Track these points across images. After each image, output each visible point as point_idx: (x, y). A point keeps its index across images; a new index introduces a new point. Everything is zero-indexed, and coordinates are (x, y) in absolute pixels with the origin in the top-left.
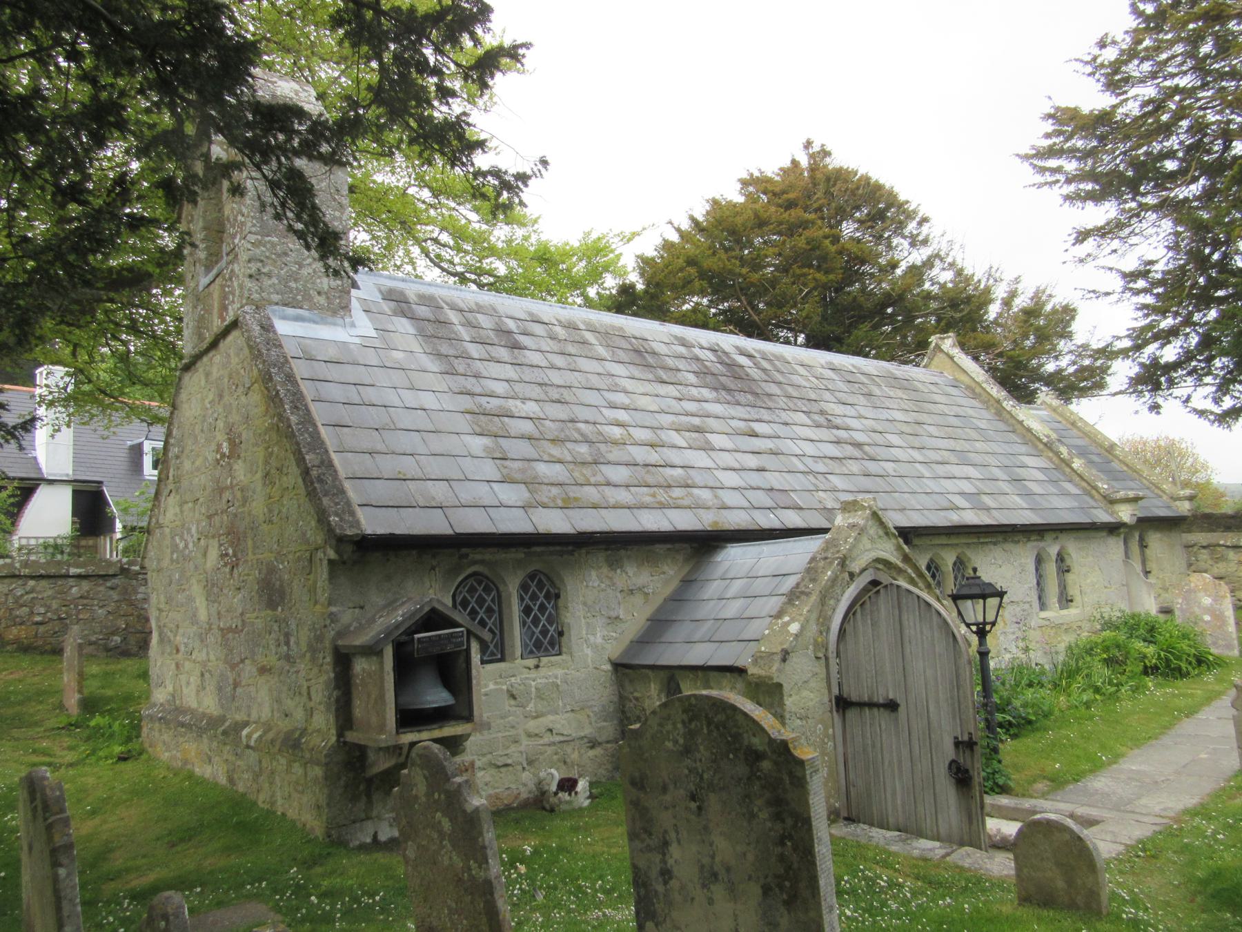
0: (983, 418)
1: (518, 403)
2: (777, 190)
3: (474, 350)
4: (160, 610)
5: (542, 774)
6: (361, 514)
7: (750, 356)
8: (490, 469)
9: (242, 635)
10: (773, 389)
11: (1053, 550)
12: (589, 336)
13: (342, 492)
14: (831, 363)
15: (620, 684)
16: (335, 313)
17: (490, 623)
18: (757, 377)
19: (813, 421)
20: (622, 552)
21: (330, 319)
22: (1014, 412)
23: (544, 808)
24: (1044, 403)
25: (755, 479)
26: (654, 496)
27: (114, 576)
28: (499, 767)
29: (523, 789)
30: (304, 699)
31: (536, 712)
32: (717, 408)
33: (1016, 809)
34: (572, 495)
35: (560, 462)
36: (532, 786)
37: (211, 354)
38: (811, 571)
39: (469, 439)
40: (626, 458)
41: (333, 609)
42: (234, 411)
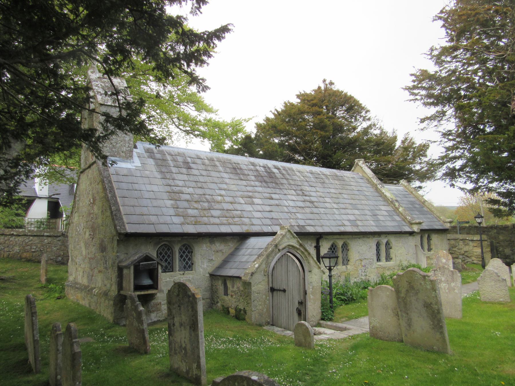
0: (369, 191)
1: (186, 188)
2: (309, 99)
3: (174, 170)
4: (72, 250)
7: (278, 169)
8: (172, 212)
11: (340, 243)
12: (217, 163)
13: (122, 219)
14: (311, 171)
15: (212, 281)
16: (127, 158)
18: (279, 177)
19: (297, 193)
20: (215, 239)
21: (126, 161)
24: (402, 184)
25: (267, 215)
26: (227, 221)
27: (60, 236)
30: (110, 281)
32: (260, 189)
33: (331, 326)
35: (197, 209)
39: (166, 201)
40: (220, 207)
41: (118, 254)
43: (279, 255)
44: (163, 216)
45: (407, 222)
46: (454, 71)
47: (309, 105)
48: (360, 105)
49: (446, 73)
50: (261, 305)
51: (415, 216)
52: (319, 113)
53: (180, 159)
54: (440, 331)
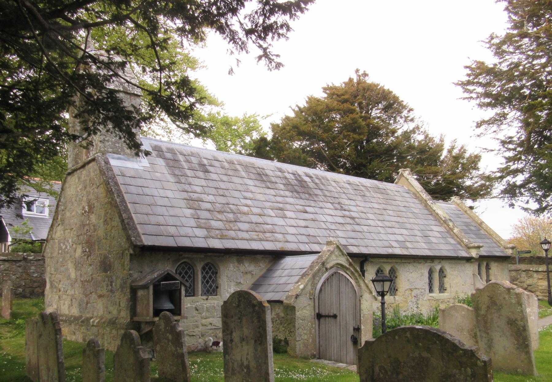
0: (417, 207)
1: (206, 196)
2: (339, 93)
3: (189, 173)
5: (207, 339)
6: (143, 237)
7: (320, 179)
8: (192, 223)
9: (91, 283)
10: (318, 192)
11: (438, 268)
12: (239, 167)
13: (136, 229)
17: (190, 281)
18: (311, 187)
19: (334, 207)
20: (244, 257)
21: (131, 159)
22: (432, 206)
23: (207, 352)
24: (454, 201)
25: (303, 231)
26: (258, 235)
27: (20, 261)
28: (190, 336)
29: (199, 345)
30: (117, 306)
31: (201, 315)
34: (224, 234)
36: (202, 344)
37: (81, 170)
38: (311, 267)
40: (248, 220)
41: (131, 272)
42: (91, 194)
43: (326, 275)
44: (183, 228)
45: (463, 245)
46: (517, 65)
47: (340, 101)
48: (400, 104)
49: (508, 66)
50: (306, 334)
51: (472, 240)
52: (352, 111)
53: (194, 160)
54: (525, 350)
